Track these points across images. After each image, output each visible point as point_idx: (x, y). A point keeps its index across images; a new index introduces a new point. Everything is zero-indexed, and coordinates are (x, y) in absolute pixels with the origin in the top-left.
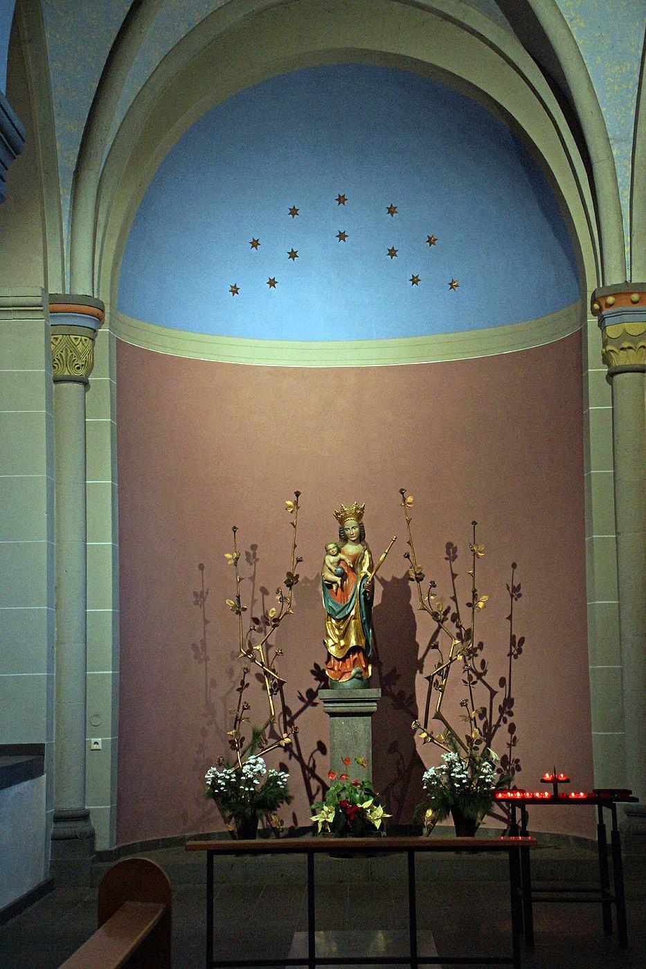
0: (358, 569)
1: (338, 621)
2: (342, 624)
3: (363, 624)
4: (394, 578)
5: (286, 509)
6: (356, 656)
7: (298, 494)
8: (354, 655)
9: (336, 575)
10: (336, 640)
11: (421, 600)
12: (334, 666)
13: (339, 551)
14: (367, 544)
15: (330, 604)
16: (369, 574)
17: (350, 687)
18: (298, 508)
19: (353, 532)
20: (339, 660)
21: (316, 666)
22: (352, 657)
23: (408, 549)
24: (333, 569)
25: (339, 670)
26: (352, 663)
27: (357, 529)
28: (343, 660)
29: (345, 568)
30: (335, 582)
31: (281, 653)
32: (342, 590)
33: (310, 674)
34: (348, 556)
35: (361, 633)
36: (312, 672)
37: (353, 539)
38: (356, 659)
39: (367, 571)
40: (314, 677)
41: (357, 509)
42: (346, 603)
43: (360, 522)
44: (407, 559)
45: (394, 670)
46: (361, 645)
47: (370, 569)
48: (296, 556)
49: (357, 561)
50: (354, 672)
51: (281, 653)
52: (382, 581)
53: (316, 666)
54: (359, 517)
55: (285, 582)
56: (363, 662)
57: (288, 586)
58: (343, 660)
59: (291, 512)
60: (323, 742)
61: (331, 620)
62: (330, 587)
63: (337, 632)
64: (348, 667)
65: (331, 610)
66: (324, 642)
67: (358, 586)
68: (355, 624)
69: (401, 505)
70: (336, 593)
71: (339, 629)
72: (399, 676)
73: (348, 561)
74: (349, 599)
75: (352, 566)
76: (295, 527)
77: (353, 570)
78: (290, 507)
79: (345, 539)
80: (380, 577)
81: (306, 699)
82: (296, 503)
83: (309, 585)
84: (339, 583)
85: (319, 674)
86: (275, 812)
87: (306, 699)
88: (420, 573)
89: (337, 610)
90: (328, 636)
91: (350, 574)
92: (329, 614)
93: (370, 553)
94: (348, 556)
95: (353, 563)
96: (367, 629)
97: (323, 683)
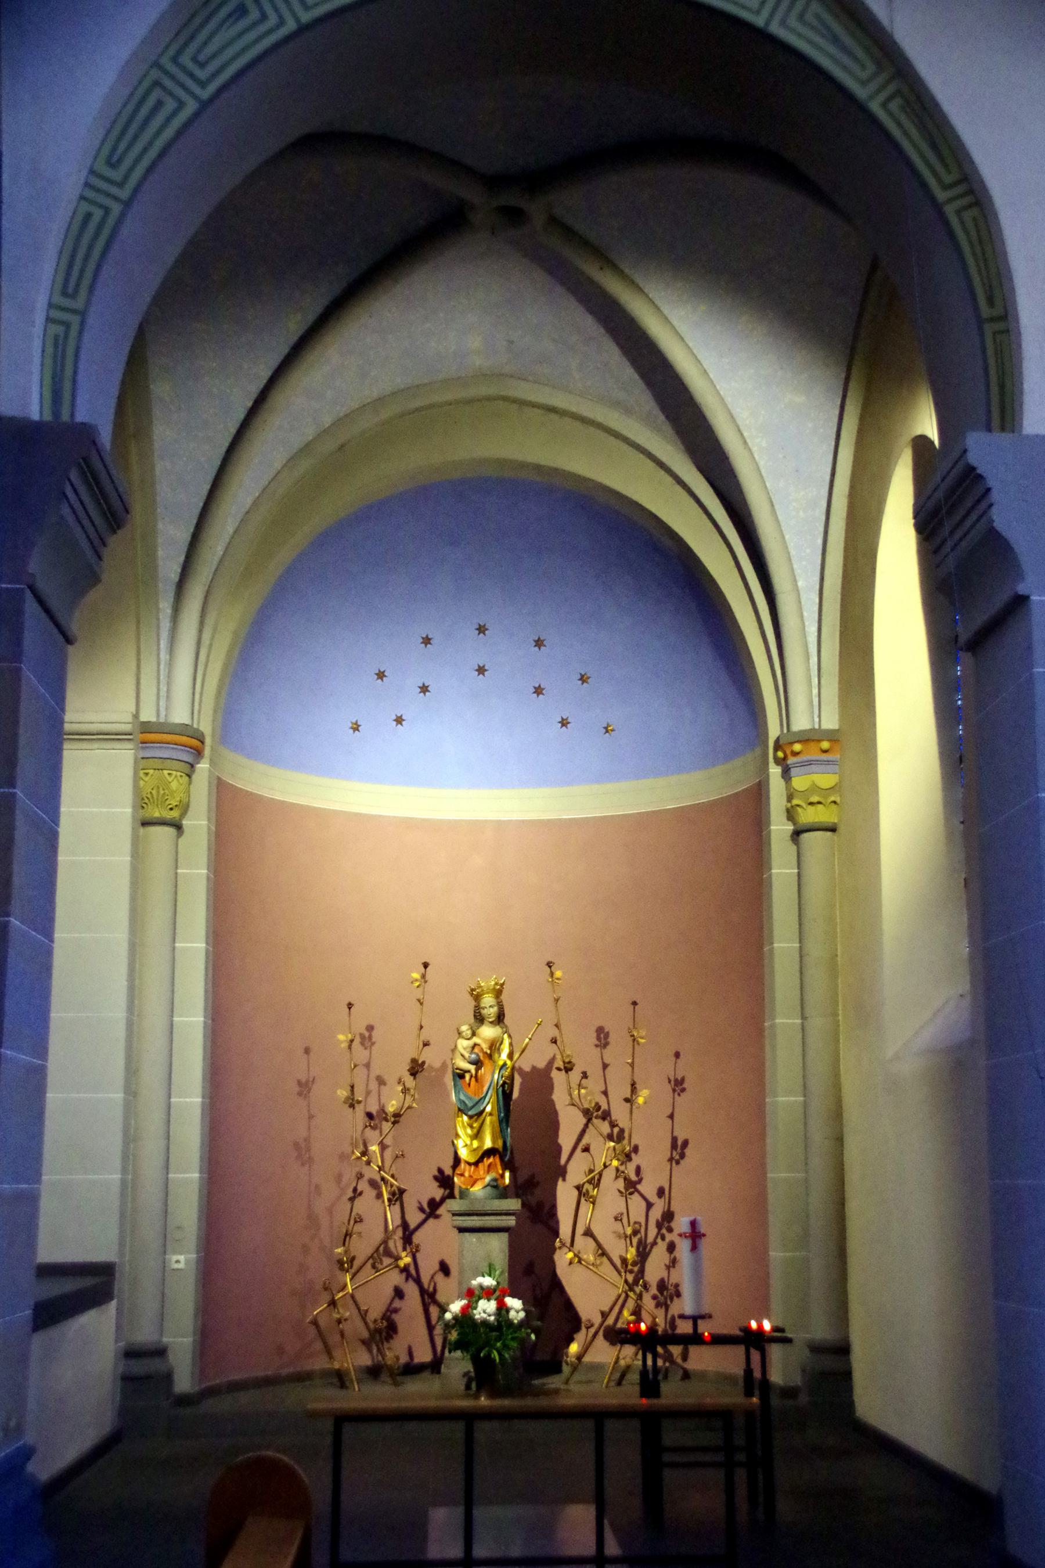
0: (496, 1055)
1: (470, 1117)
2: (476, 1121)
3: (500, 1122)
4: (534, 1068)
6: (491, 1160)
8: (489, 1157)
11: (570, 1095)
13: (474, 1034)
15: (462, 1097)
16: (509, 1063)
18: (426, 982)
19: (491, 1012)
20: (470, 1164)
22: (487, 1162)
23: (555, 1032)
24: (467, 1055)
25: (471, 1176)
28: (476, 1164)
29: (481, 1055)
30: (469, 1071)
32: (477, 1080)
34: (484, 1040)
35: (498, 1134)
36: (436, 1178)
41: (496, 984)
45: (533, 1176)
47: (510, 1056)
48: (422, 1038)
49: (495, 1046)
50: (488, 1179)
52: (521, 1071)
54: (498, 993)
56: (499, 1167)
57: (412, 1074)
58: (476, 1164)
62: (462, 1076)
63: (469, 1131)
64: (482, 1172)
68: (491, 1122)
71: (471, 1127)
76: (421, 1004)
77: (490, 1057)
78: (417, 980)
79: (480, 1019)
82: (423, 976)
84: (473, 1072)
88: (570, 1062)
89: (470, 1104)
90: (457, 1136)
91: (487, 1062)
92: (460, 1110)
93: (510, 1036)
94: (484, 1040)
95: (490, 1048)
97: (447, 1191)
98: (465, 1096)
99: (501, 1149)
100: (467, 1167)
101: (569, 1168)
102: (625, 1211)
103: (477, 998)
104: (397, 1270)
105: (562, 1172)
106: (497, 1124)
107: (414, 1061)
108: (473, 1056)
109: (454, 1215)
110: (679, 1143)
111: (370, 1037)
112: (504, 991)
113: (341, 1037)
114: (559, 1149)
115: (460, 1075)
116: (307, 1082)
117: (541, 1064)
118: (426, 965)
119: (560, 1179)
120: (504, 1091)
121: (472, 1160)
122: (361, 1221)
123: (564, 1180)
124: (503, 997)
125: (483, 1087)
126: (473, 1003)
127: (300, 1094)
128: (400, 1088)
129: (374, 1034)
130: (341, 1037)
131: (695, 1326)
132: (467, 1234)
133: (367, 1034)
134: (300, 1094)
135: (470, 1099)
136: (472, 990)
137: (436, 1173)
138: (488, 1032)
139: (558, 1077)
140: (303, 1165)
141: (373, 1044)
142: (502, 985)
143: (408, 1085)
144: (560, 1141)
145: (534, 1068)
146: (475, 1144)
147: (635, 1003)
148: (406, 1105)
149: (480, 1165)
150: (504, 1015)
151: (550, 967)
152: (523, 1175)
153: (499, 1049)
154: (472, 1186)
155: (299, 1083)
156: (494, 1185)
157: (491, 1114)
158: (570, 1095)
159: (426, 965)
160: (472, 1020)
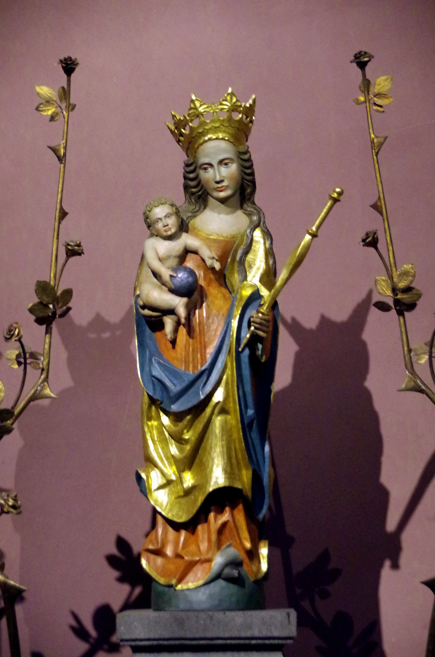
0: (236, 277)
1: (177, 417)
2: (190, 426)
3: (246, 427)
4: (324, 321)
5: (37, 109)
6: (226, 517)
7: (69, 66)
8: (220, 511)
9: (172, 291)
10: (171, 472)
11: (410, 366)
12: (164, 545)
13: (183, 227)
14: (259, 212)
15: (157, 372)
16: (264, 292)
17: (205, 606)
18: (71, 107)
19: (223, 175)
20: (176, 526)
21: (122, 544)
22: (216, 521)
23: (374, 223)
24: (166, 273)
25: (178, 556)
26: (214, 537)
27: (234, 167)
28: (190, 526)
29: (200, 273)
30: (171, 312)
31: (14, 507)
32: (190, 332)
33: (105, 564)
34: (208, 241)
35: (242, 454)
36: (112, 560)
37: (222, 194)
38: (224, 525)
39: (259, 284)
40: (115, 574)
41: (234, 108)
42: (200, 368)
43: (242, 149)
44: (372, 250)
45: (325, 556)
46: (238, 485)
47: (269, 277)
48: (63, 239)
49: (233, 255)
50: (218, 560)
51: (14, 507)
52: (295, 328)
53: (122, 544)
54: (240, 132)
55: (31, 310)
56: (245, 534)
57: (39, 321)
58: (190, 526)
59: (52, 118)
60: (259, 280)
61: (159, 418)
62: (157, 325)
63: (174, 450)
64: (204, 546)
65: (158, 387)
66: (139, 478)
67: (235, 324)
68: (225, 428)
69: (358, 103)
70: (173, 342)
71: (179, 440)
72: (337, 573)
73: (207, 253)
74: (209, 358)
75: (217, 266)
76: (61, 159)
77: (221, 277)
78: (48, 102)
79: (198, 194)
80: (289, 320)
81: (93, 633)
82: (65, 94)
83: (107, 335)
84: (182, 312)
85: (125, 562)
86: (389, 80)
87: (93, 633)
88: (408, 290)
89: (174, 387)
90: (149, 462)
91: (215, 293)
92: (153, 401)
93: (267, 234)
94: (208, 241)
95: (222, 259)
96: (257, 442)
97: (138, 590)
98: (166, 368)
100: (171, 532)
101: (406, 538)
105: (390, 549)
106: (238, 434)
107: (43, 288)
108: (181, 275)
112: (254, 129)
114: (383, 495)
115: (152, 320)
117: (340, 314)
119: (387, 564)
120: (253, 359)
121: (182, 518)
123: (395, 566)
124: (252, 143)
126: (179, 156)
128: (13, 352)
135: (173, 373)
136: (180, 124)
137: (114, 550)
139: (380, 332)
142: (249, 111)
143: (30, 347)
144: (385, 479)
145: (324, 321)
146: (189, 479)
148: (28, 393)
149: (200, 528)
151: (362, 65)
152: (302, 558)
153: (242, 262)
154: (180, 581)
156: (233, 575)
157: (224, 410)
158: (410, 366)
160: (180, 197)
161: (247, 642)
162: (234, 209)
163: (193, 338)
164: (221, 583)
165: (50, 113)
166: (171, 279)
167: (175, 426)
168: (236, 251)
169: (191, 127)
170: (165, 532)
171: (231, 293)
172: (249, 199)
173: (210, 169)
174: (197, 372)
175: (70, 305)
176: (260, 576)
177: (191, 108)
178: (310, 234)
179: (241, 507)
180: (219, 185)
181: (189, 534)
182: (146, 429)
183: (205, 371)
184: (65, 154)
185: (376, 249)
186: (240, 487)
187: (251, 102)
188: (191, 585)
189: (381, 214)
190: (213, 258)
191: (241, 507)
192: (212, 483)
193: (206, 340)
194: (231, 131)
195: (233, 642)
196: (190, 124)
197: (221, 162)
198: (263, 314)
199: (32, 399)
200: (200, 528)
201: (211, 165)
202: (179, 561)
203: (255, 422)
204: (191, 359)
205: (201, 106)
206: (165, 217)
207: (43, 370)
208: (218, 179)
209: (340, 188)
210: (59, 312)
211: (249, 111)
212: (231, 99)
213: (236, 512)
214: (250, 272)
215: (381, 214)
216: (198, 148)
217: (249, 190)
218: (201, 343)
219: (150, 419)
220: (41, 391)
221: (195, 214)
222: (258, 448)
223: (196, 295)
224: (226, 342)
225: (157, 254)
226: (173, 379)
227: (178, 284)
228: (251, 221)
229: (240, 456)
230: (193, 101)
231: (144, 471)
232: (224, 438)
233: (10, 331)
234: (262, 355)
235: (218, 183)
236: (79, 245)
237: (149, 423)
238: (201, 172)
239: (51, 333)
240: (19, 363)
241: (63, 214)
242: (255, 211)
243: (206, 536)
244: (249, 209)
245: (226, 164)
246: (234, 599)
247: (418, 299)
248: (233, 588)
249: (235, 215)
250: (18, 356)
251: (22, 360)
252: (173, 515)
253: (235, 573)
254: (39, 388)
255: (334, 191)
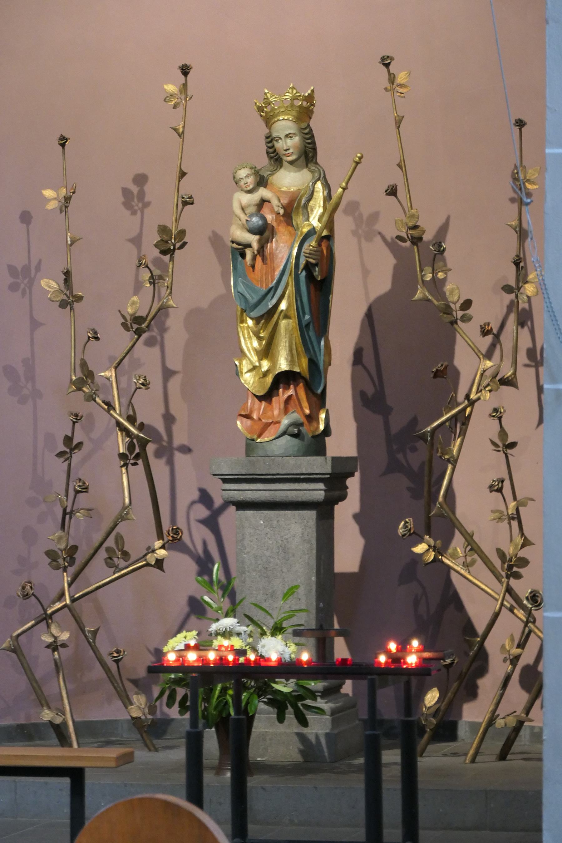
6: (291, 392)
8: (287, 388)
12: (251, 412)
19: (290, 145)
22: (283, 394)
23: (397, 178)
26: (282, 406)
30: (249, 246)
31: (143, 384)
35: (301, 349)
37: (290, 159)
38: (290, 397)
41: (295, 98)
42: (270, 286)
46: (297, 370)
50: (285, 422)
51: (143, 384)
55: (156, 246)
56: (305, 404)
63: (256, 344)
64: (276, 412)
70: (253, 266)
76: (181, 135)
79: (276, 159)
84: (255, 246)
88: (415, 227)
89: (253, 299)
93: (327, 186)
96: (314, 339)
98: (246, 286)
99: (306, 373)
102: (506, 476)
103: (269, 121)
104: (69, 567)
107: (163, 230)
108: (255, 220)
109: (225, 481)
110: (21, 371)
111: (141, 195)
113: (48, 193)
116: (26, 269)
118: (185, 70)
120: (310, 277)
122: (85, 489)
125: (274, 270)
127: (13, 287)
129: (147, 188)
130: (48, 193)
131: (214, 650)
132: (249, 513)
133: (135, 189)
134: (13, 287)
136: (260, 109)
138: (289, 180)
140: (23, 401)
141: (147, 205)
142: (310, 98)
146: (265, 365)
147: (520, 124)
150: (315, 150)
151: (387, 65)
154: (259, 436)
155: (12, 270)
159: (185, 70)
161: (298, 476)
162: (300, 168)
163: (266, 264)
164: (287, 438)
165: (173, 102)
166: (247, 223)
167: (256, 327)
168: (300, 200)
169: (266, 112)
170: (253, 403)
171: (296, 230)
172: (312, 161)
173: (280, 141)
174: (268, 289)
175: (185, 240)
176: (317, 433)
177: (265, 99)
178: (342, 188)
179: (301, 384)
180: (287, 152)
181: (267, 404)
182: (239, 329)
183: (272, 288)
184: (183, 132)
185: (396, 197)
186: (298, 371)
187: (309, 92)
188: (266, 439)
189: (402, 171)
190: (279, 206)
191: (301, 384)
192: (277, 368)
193: (275, 265)
194: (294, 113)
195: (289, 477)
196: (265, 109)
197: (287, 136)
198: (313, 247)
199: (159, 310)
200: (274, 399)
201: (281, 138)
202: (259, 422)
203: (311, 324)
204: (264, 279)
205: (271, 96)
206: (246, 177)
207: (168, 287)
208: (285, 148)
209: (360, 153)
210: (178, 245)
211: (310, 98)
212: (292, 91)
213: (298, 388)
214: (312, 214)
215: (402, 171)
216: (271, 126)
217: (311, 155)
218: (271, 267)
219: (242, 322)
220: (166, 302)
221: (273, 172)
222: (315, 343)
223: (267, 234)
224: (288, 267)
225: (241, 204)
226: (252, 294)
227: (251, 227)
228: (313, 177)
229: (300, 349)
230: (265, 94)
231: (237, 360)
232: (287, 336)
233: (139, 261)
234: (318, 276)
235: (286, 150)
236: (191, 197)
237: (241, 325)
238: (275, 143)
239: (173, 261)
240: (150, 283)
241: (183, 174)
242: (317, 169)
243: (278, 405)
244: (312, 168)
245: (291, 137)
246: (296, 449)
247: (423, 234)
248: (295, 441)
249: (301, 172)
250: (150, 278)
251: (152, 281)
252: (256, 391)
253: (296, 431)
254: (165, 300)
255: (356, 156)
